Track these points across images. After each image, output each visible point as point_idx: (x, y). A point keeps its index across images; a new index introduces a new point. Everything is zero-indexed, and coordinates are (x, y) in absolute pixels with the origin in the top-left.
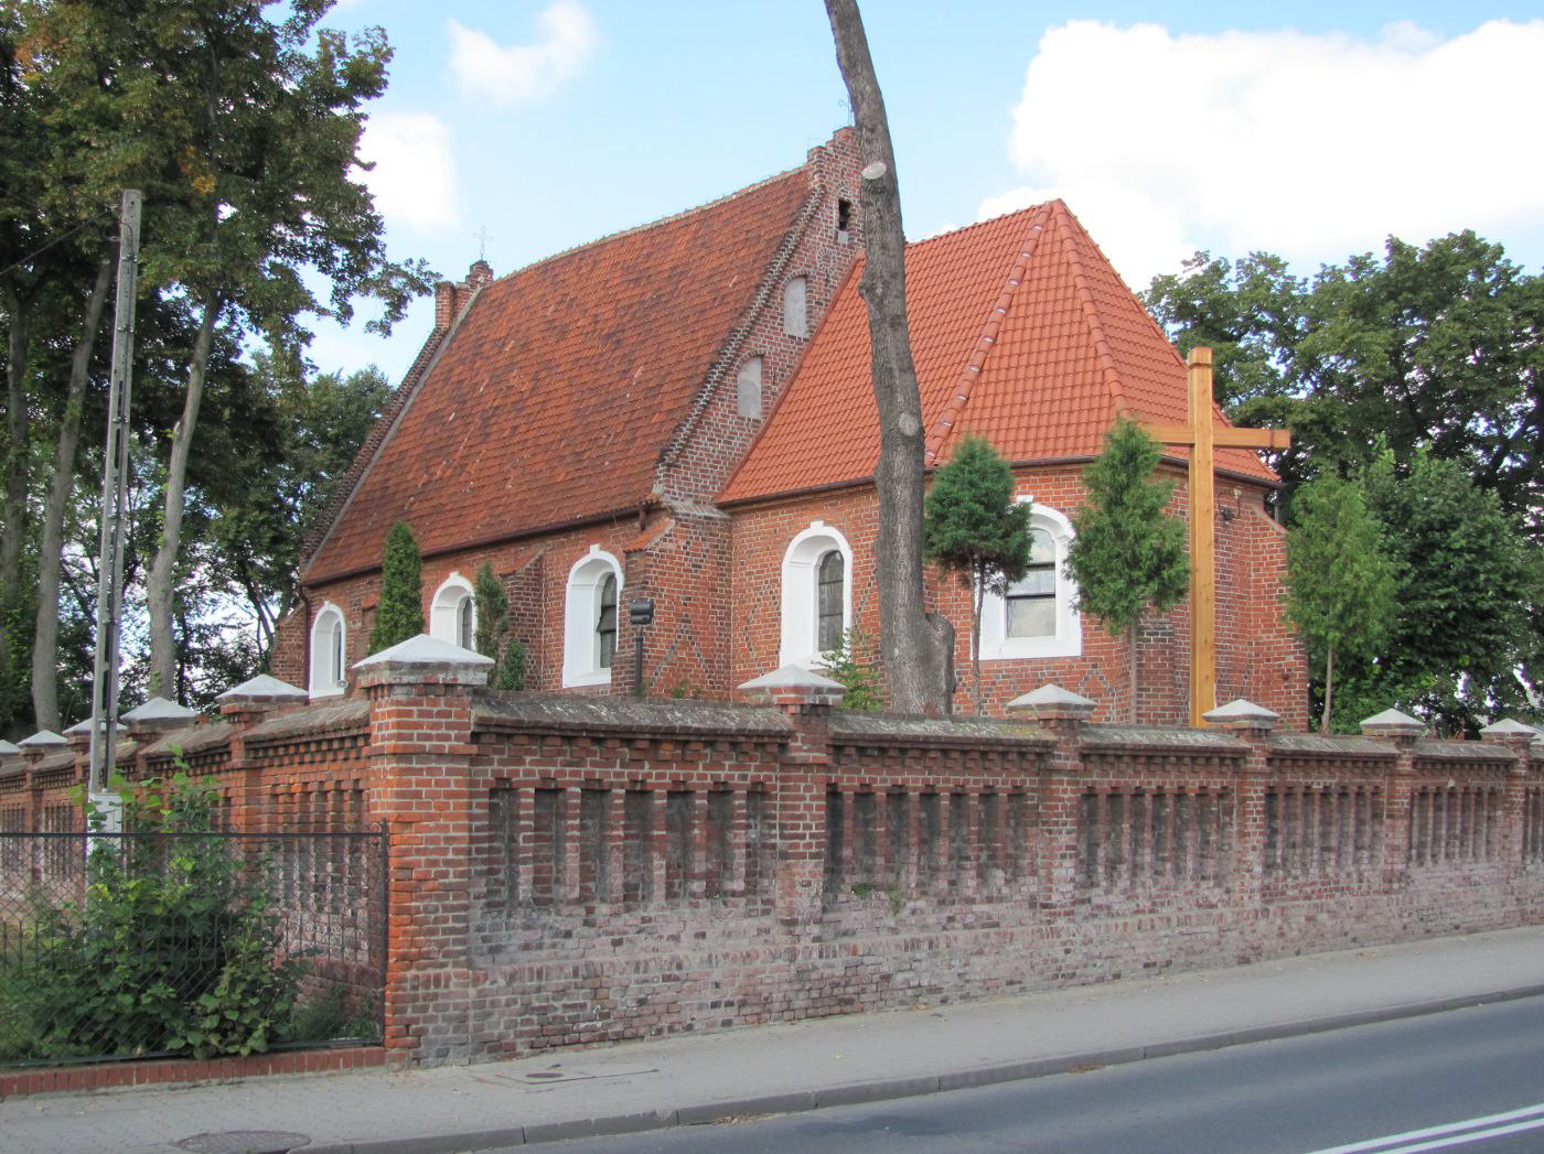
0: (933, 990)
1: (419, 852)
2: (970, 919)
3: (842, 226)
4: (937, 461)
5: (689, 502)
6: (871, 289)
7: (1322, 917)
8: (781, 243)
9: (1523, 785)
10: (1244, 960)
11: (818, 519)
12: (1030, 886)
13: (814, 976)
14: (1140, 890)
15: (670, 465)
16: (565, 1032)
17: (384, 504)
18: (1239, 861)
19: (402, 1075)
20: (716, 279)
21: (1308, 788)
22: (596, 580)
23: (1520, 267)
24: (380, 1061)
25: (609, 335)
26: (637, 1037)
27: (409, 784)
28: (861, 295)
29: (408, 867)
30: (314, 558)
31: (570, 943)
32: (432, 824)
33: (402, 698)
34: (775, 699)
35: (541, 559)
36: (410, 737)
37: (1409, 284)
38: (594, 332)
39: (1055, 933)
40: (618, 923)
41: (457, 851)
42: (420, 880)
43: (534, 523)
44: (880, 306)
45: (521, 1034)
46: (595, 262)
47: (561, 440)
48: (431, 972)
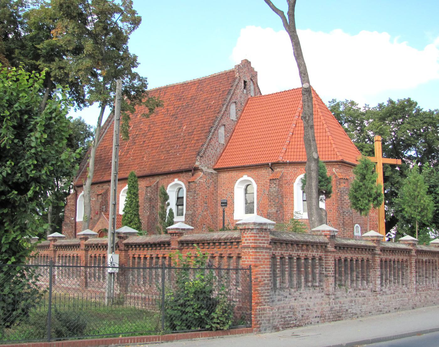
0: (356, 314)
1: (260, 274)
2: (360, 294)
3: (245, 88)
4: (283, 160)
5: (206, 168)
6: (305, 118)
7: (428, 296)
8: (229, 92)
9: (379, 257)
10: (413, 308)
11: (246, 175)
12: (371, 285)
13: (334, 309)
14: (391, 288)
15: (201, 157)
16: (288, 324)
17: (101, 162)
18: (411, 280)
19: (257, 335)
20: (207, 101)
21: (422, 260)
22: (176, 189)
23: (422, 109)
24: (252, 331)
25: (173, 115)
26: (302, 326)
27: (257, 255)
28: (302, 119)
29: (257, 278)
30: (78, 178)
31: (287, 299)
32: (262, 266)
33: (255, 232)
34: (323, 233)
35: (158, 182)
36: (257, 243)
37: (395, 113)
38: (168, 114)
39: (377, 299)
40: (295, 294)
41: (267, 274)
42: (259, 282)
43: (156, 171)
44: (307, 122)
45: (280, 325)
46: (165, 93)
47: (161, 146)
48: (262, 307)
